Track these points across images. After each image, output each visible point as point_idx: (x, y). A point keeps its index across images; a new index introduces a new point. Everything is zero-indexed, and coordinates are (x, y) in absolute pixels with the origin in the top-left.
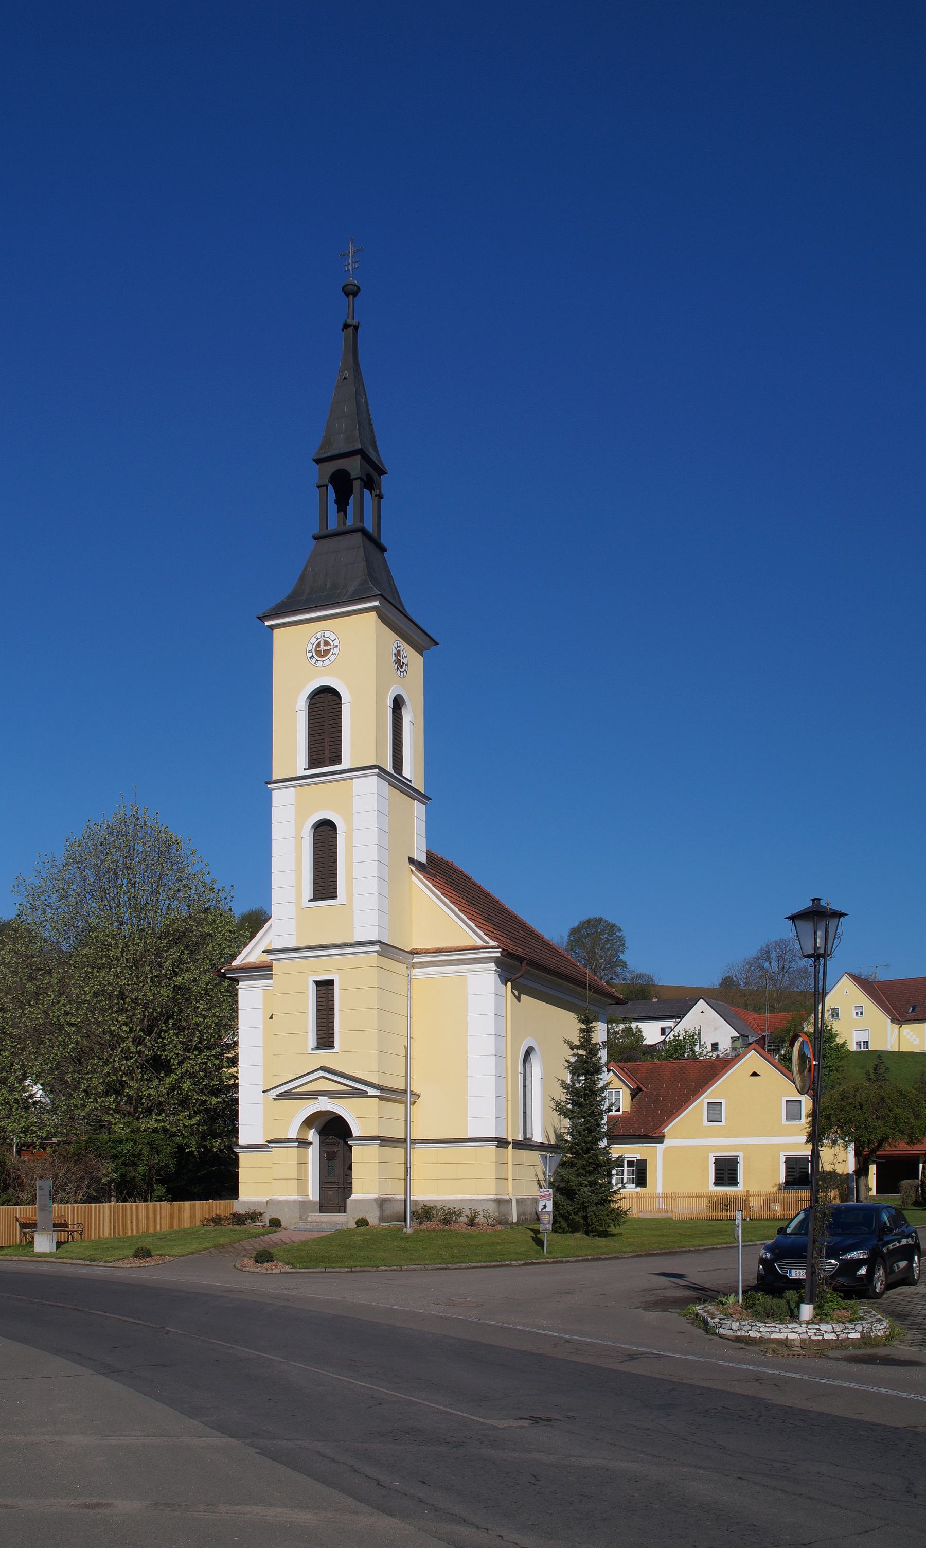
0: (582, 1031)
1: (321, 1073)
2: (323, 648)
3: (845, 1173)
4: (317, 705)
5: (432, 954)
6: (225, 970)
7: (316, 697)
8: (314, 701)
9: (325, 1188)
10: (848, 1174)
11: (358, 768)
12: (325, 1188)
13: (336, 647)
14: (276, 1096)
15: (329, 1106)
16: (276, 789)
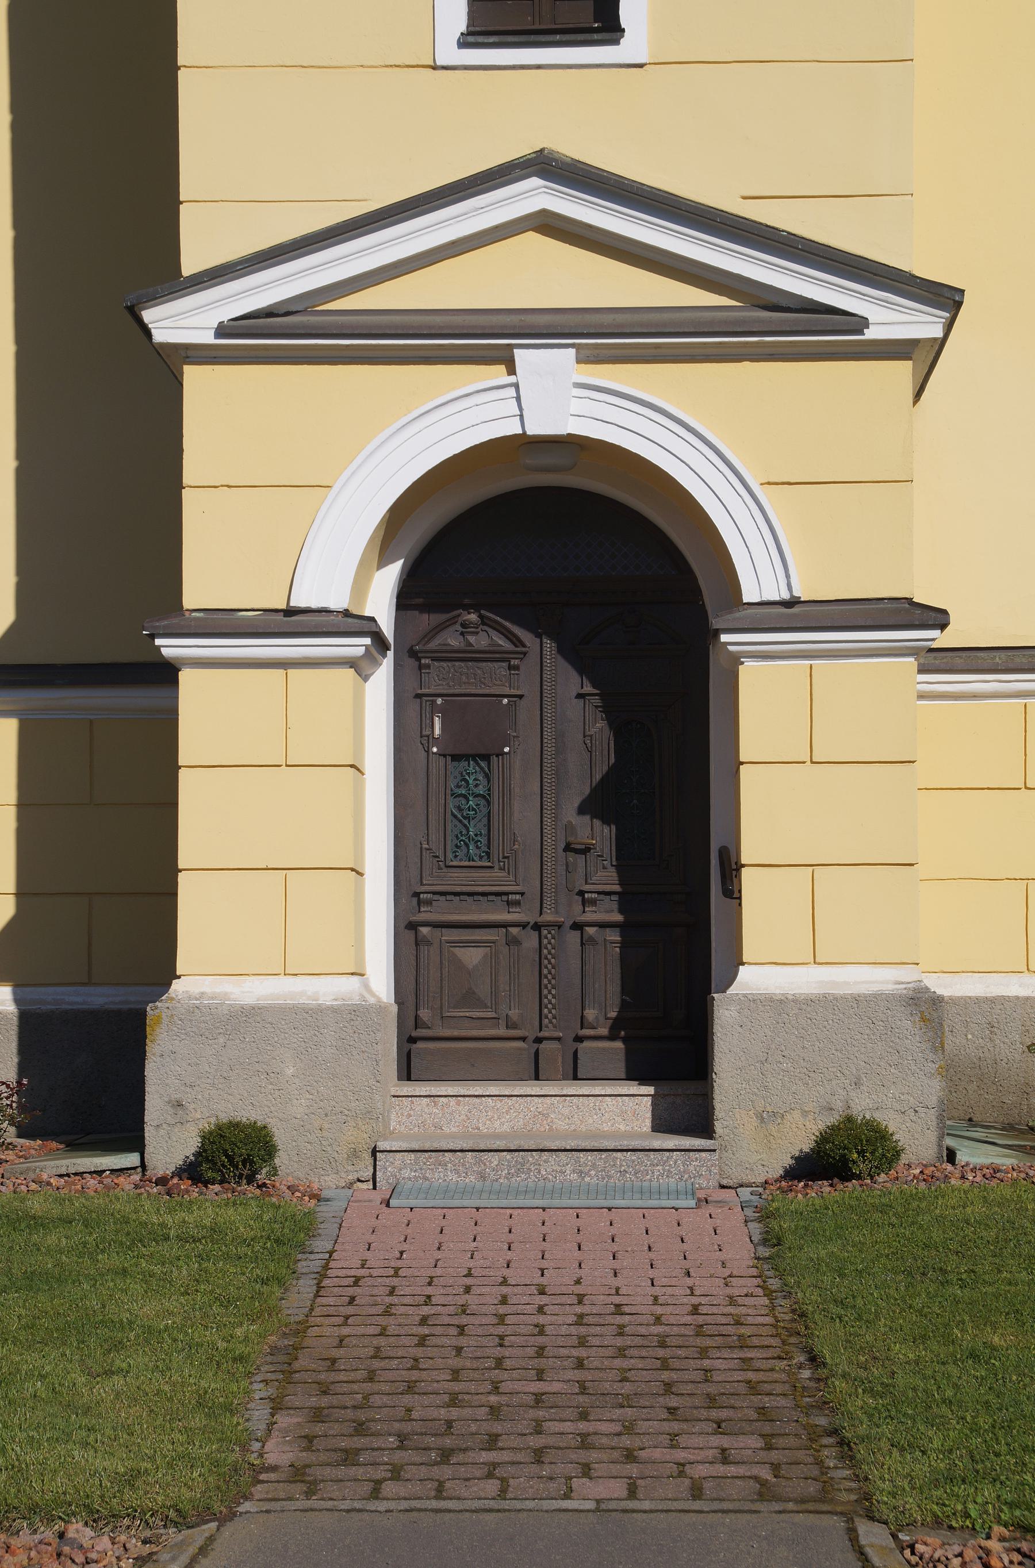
14: (222, 331)
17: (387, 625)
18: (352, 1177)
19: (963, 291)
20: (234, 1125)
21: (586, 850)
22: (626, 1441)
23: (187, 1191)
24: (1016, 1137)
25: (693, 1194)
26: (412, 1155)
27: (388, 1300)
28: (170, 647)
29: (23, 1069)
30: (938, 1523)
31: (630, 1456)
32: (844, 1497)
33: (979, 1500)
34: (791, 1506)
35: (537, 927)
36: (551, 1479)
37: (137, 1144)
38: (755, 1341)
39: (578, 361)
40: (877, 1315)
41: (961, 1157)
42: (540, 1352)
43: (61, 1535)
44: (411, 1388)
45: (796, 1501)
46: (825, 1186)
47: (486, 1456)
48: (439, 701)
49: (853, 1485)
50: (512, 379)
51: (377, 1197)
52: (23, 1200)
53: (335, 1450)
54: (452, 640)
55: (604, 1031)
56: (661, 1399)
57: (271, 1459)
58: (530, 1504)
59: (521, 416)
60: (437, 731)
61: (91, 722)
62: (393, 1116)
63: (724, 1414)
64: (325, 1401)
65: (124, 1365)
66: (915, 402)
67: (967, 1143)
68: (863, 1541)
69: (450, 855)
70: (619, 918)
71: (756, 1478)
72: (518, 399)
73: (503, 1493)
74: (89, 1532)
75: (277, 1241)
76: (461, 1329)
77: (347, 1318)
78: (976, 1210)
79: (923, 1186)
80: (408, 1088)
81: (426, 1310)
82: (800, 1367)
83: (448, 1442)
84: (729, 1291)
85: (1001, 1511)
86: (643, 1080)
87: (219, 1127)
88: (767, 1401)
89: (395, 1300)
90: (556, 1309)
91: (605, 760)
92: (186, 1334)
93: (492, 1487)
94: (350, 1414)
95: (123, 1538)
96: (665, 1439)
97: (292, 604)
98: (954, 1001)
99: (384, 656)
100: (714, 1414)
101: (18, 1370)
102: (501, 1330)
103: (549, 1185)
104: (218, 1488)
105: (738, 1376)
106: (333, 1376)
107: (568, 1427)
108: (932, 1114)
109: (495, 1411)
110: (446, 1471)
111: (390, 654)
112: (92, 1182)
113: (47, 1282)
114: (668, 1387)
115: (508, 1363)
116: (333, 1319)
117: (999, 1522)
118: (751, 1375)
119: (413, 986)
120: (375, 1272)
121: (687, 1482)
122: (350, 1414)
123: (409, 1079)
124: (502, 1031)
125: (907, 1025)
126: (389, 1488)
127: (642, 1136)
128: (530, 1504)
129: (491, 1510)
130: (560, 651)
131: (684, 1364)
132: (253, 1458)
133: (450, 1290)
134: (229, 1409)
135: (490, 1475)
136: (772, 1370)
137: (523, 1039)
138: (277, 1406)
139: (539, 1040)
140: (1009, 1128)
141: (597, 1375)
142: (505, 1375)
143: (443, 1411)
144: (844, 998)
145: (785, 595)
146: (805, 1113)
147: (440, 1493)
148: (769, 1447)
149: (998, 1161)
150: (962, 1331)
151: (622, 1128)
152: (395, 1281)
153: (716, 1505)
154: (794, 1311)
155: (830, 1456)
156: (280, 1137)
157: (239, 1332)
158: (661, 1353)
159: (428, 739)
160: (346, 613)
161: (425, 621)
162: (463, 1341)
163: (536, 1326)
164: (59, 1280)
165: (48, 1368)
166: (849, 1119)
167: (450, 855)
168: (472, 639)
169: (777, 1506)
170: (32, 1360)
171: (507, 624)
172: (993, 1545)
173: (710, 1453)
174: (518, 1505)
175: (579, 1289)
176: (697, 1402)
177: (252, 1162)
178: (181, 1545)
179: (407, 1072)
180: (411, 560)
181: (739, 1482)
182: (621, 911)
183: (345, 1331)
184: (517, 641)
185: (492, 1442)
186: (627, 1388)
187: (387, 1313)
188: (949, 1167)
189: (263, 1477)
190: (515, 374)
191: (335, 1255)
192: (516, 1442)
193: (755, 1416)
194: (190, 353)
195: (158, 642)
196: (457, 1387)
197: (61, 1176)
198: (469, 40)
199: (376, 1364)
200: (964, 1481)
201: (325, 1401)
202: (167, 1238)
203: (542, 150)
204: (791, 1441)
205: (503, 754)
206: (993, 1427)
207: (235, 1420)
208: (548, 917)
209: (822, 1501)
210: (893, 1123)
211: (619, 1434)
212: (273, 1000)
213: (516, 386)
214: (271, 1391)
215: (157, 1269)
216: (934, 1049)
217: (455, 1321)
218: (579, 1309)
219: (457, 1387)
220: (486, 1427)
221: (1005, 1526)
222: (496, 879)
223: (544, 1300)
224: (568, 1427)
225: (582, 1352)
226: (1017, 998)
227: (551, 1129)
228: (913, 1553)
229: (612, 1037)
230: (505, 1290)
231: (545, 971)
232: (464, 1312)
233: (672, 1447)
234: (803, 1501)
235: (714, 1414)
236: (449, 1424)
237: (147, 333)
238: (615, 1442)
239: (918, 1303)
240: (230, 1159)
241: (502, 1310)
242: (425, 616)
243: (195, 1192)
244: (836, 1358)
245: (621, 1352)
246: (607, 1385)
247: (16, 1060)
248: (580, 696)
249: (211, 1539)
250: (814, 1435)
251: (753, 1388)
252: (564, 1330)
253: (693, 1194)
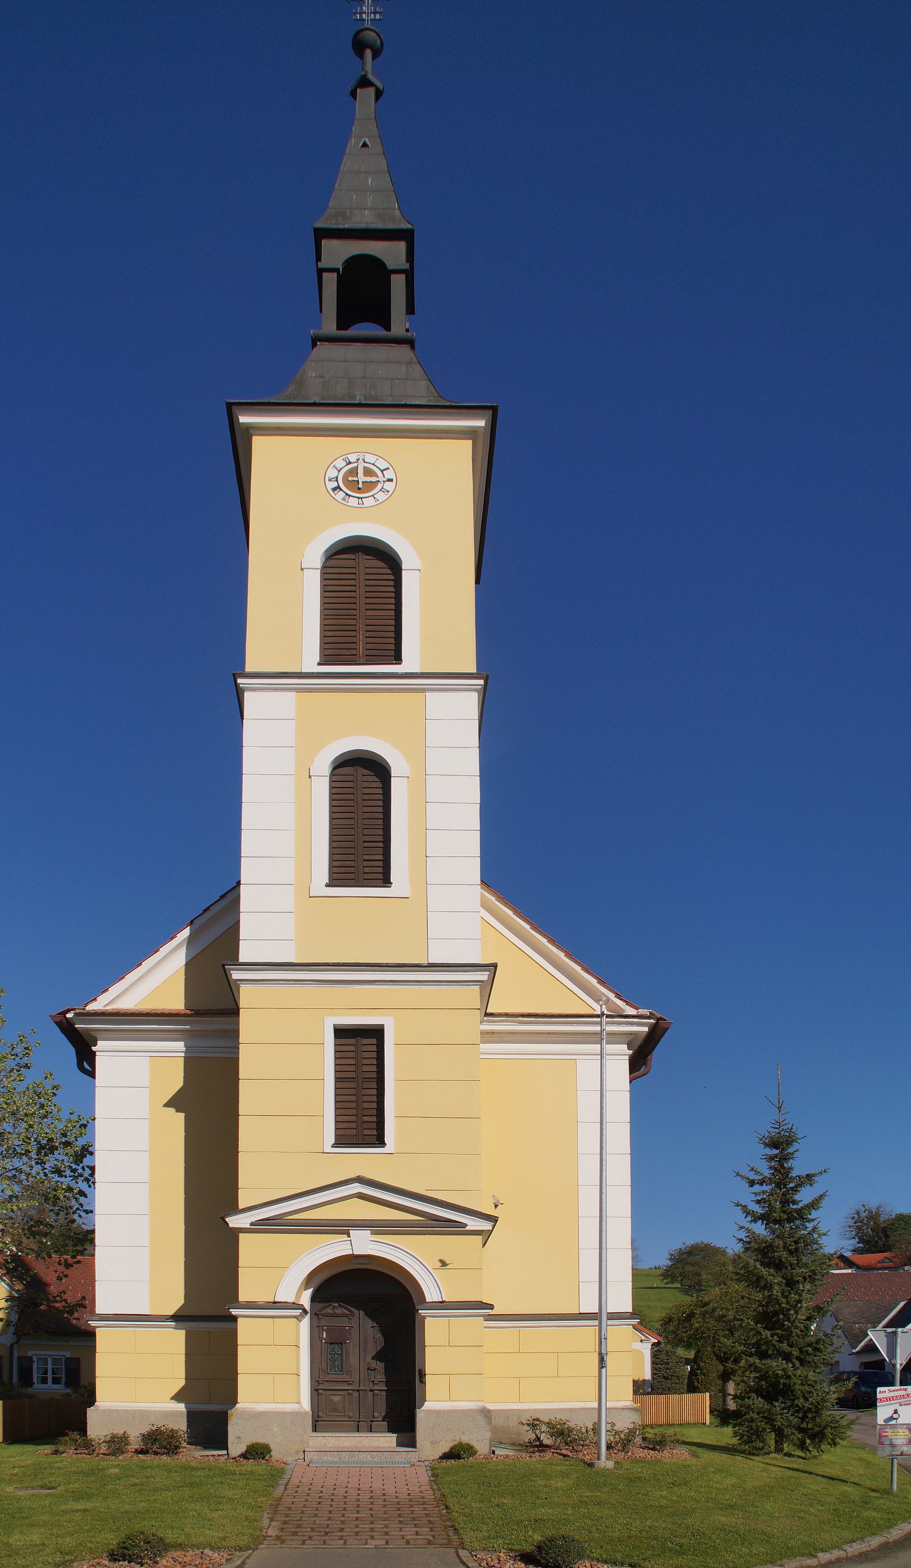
0: (771, 1158)
1: (357, 1188)
2: (362, 478)
3: (641, 1379)
4: (338, 570)
5: (520, 1018)
6: (76, 1014)
7: (336, 557)
8: (332, 563)
9: (324, 1390)
10: (644, 1380)
11: (448, 673)
12: (324, 1390)
13: (390, 480)
14: (252, 1224)
15: (370, 1246)
16: (254, 690)
17: (307, 1306)
18: (296, 1458)
19: (498, 1217)
20: (257, 1444)
21: (375, 1370)
22: (386, 1530)
23: (242, 1461)
24: (515, 1447)
25: (410, 1463)
26: (317, 1453)
27: (308, 1492)
28: (234, 1312)
29: (188, 1427)
30: (484, 1549)
31: (387, 1534)
32: (455, 1543)
33: (497, 1543)
34: (438, 1546)
35: (358, 1391)
36: (361, 1540)
37: (226, 1447)
38: (428, 1503)
39: (371, 1234)
40: (468, 1496)
41: (496, 1453)
42: (358, 1506)
43: (202, 1553)
44: (315, 1515)
45: (440, 1545)
46: (453, 1461)
47: (339, 1534)
48: (325, 1328)
49: (458, 1540)
50: (349, 1239)
51: (305, 1464)
52: (189, 1462)
53: (290, 1532)
54: (329, 1310)
55: (381, 1419)
56: (397, 1519)
57: (270, 1534)
58: (354, 1546)
59: (352, 1249)
60: (324, 1336)
61: (209, 1331)
62: (310, 1442)
63: (417, 1522)
64: (287, 1519)
65: (222, 1508)
66: (483, 1247)
67: (499, 1448)
68: (460, 1555)
69: (329, 1370)
70: (386, 1388)
71: (427, 1539)
72: (351, 1244)
73: (345, 1544)
74: (211, 1552)
75: (272, 1475)
76: (332, 1500)
77: (295, 1496)
78: (500, 1467)
79: (484, 1461)
80: (315, 1434)
81: (321, 1495)
82: (443, 1509)
83: (327, 1530)
84: (420, 1489)
85: (504, 1545)
86: (393, 1432)
87: (253, 1444)
88: (431, 1519)
89: (310, 1492)
90: (364, 1495)
91: (381, 1344)
92: (242, 1500)
93: (342, 1542)
94: (295, 1522)
95: (222, 1554)
96: (398, 1529)
97: (275, 1300)
98: (495, 1410)
99: (307, 1315)
100: (414, 1522)
101: (188, 1509)
102: (345, 1500)
103: (362, 1461)
104: (253, 1541)
105: (423, 1512)
106: (290, 1512)
107: (367, 1526)
108: (488, 1442)
109: (343, 1522)
110: (327, 1538)
111: (309, 1315)
112: (212, 1458)
113: (197, 1485)
114: (400, 1515)
115: (347, 1509)
116: (290, 1497)
117: (504, 1548)
118: (426, 1512)
119: (317, 1406)
120: (304, 1484)
121: (405, 1540)
122: (295, 1522)
123: (316, 1431)
124: (347, 1419)
125: (480, 1418)
126: (308, 1542)
127: (392, 1448)
128: (354, 1546)
129: (341, 1548)
130: (366, 1314)
131: (405, 1509)
132: (264, 1534)
133: (329, 1489)
134: (256, 1520)
135: (341, 1539)
136: (434, 1510)
137: (354, 1421)
138: (272, 1520)
139: (359, 1421)
140: (513, 1444)
141: (376, 1512)
142: (347, 1512)
143: (326, 1522)
144: (459, 1410)
145: (441, 1300)
146: (446, 1441)
147: (324, 1543)
148: (432, 1531)
149: (508, 1453)
150: (495, 1499)
151: (386, 1445)
152: (311, 1487)
153: (414, 1546)
154: (441, 1495)
155: (451, 1533)
156: (272, 1447)
157: (259, 1500)
158: (397, 1506)
159: (322, 1338)
160: (293, 1303)
161: (320, 1305)
162: (333, 1503)
163: (357, 1499)
164: (201, 1484)
165: (197, 1508)
166: (461, 1443)
167: (329, 1370)
168: (336, 1311)
169: (434, 1546)
170: (193, 1506)
171: (348, 1306)
172: (501, 1554)
173: (412, 1533)
174: (350, 1547)
175: (371, 1489)
176: (409, 1519)
177: (263, 1454)
178: (241, 1556)
179: (315, 1429)
180: (315, 1289)
181: (422, 1540)
182: (386, 1386)
183: (294, 1500)
184: (351, 1312)
185: (342, 1530)
186: (386, 1516)
187: (308, 1495)
188: (493, 1455)
189: (267, 1539)
190: (350, 1237)
191: (291, 1479)
192: (348, 1530)
193: (428, 1523)
194: (242, 1230)
195: (230, 1310)
196: (330, 1515)
197: (201, 1456)
198: (337, 1144)
199: (304, 1509)
200: (493, 1539)
201: (287, 1519)
202: (236, 1474)
203: (359, 1176)
204: (439, 1529)
205: (347, 1343)
206: (503, 1524)
207: (258, 1523)
208: (362, 1388)
209: (448, 1545)
210: (474, 1444)
211: (383, 1528)
212: (85, 1019)
213: (351, 1241)
214: (270, 1516)
215: (233, 1482)
216: (488, 1424)
217: (330, 1497)
218: (371, 1495)
219: (330, 1515)
220: (340, 1526)
221: (505, 1549)
222: (345, 1377)
223: (359, 1492)
224: (367, 1526)
225: (372, 1506)
226: (516, 1409)
227: (363, 1446)
228: (476, 1557)
229: (383, 1420)
230: (347, 1489)
231: (361, 1403)
232: (333, 1495)
233: (400, 1531)
234: (442, 1545)
235: (414, 1522)
236: (328, 1525)
237: (228, 1224)
238: (382, 1530)
239: (481, 1492)
240: (257, 1453)
241: (346, 1495)
242: (320, 1304)
243: (245, 1461)
244: (454, 1507)
245: (385, 1506)
246: (380, 1515)
247: (186, 1424)
248: (372, 1327)
249: (250, 1555)
250: (446, 1527)
251: (427, 1515)
252: (366, 1500)
253: (410, 1463)
